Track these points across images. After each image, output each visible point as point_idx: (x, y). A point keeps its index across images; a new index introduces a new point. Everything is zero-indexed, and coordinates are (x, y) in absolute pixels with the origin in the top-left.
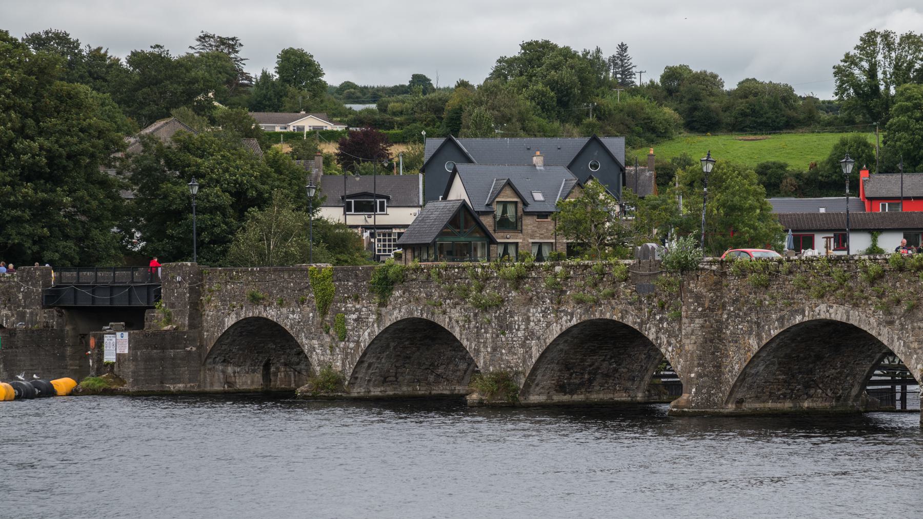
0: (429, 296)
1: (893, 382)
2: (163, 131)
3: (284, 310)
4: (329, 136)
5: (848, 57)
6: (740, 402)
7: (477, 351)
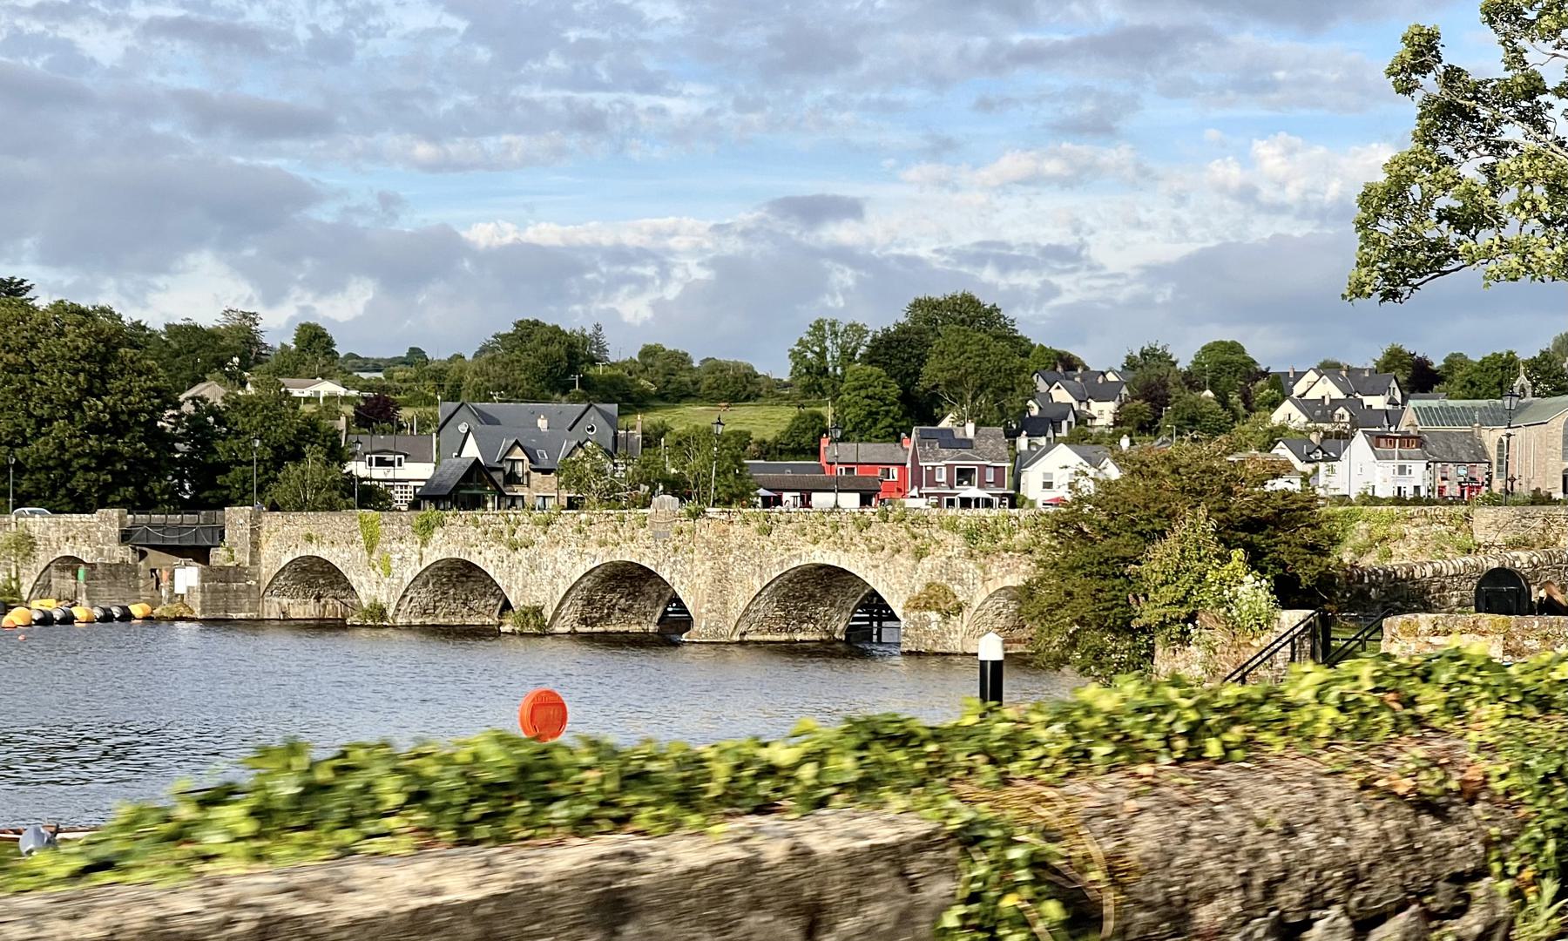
0: (467, 538)
1: (871, 620)
2: (213, 391)
3: (335, 550)
4: (345, 400)
5: (801, 342)
6: (743, 634)
7: (509, 588)
